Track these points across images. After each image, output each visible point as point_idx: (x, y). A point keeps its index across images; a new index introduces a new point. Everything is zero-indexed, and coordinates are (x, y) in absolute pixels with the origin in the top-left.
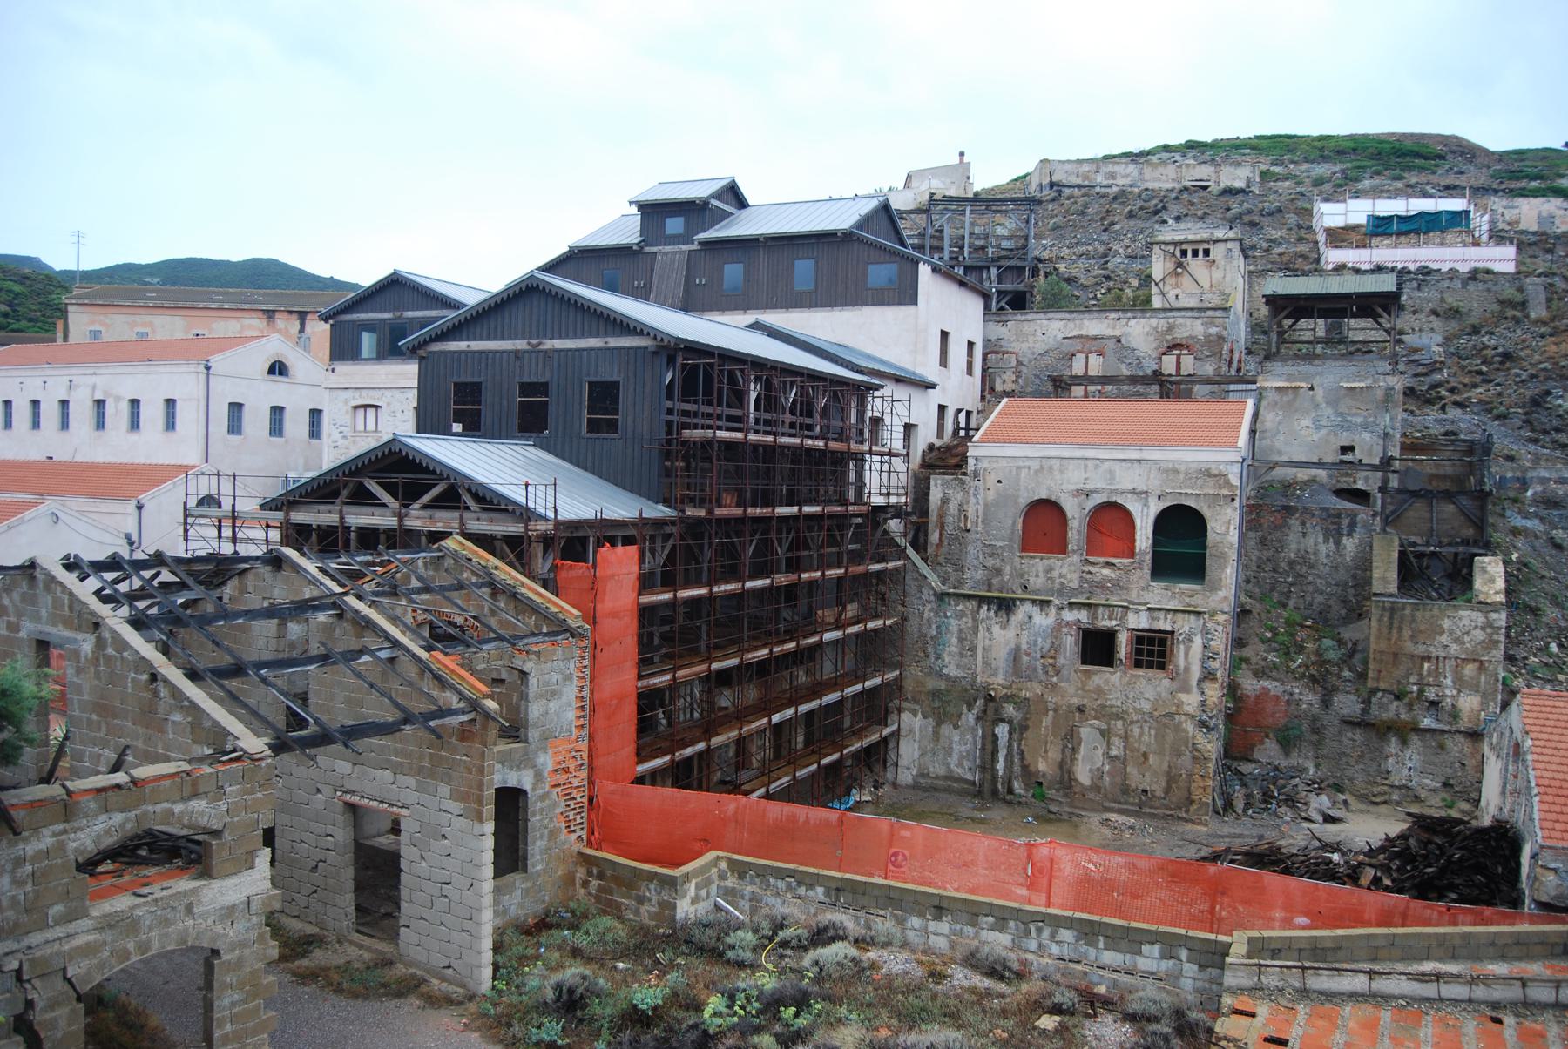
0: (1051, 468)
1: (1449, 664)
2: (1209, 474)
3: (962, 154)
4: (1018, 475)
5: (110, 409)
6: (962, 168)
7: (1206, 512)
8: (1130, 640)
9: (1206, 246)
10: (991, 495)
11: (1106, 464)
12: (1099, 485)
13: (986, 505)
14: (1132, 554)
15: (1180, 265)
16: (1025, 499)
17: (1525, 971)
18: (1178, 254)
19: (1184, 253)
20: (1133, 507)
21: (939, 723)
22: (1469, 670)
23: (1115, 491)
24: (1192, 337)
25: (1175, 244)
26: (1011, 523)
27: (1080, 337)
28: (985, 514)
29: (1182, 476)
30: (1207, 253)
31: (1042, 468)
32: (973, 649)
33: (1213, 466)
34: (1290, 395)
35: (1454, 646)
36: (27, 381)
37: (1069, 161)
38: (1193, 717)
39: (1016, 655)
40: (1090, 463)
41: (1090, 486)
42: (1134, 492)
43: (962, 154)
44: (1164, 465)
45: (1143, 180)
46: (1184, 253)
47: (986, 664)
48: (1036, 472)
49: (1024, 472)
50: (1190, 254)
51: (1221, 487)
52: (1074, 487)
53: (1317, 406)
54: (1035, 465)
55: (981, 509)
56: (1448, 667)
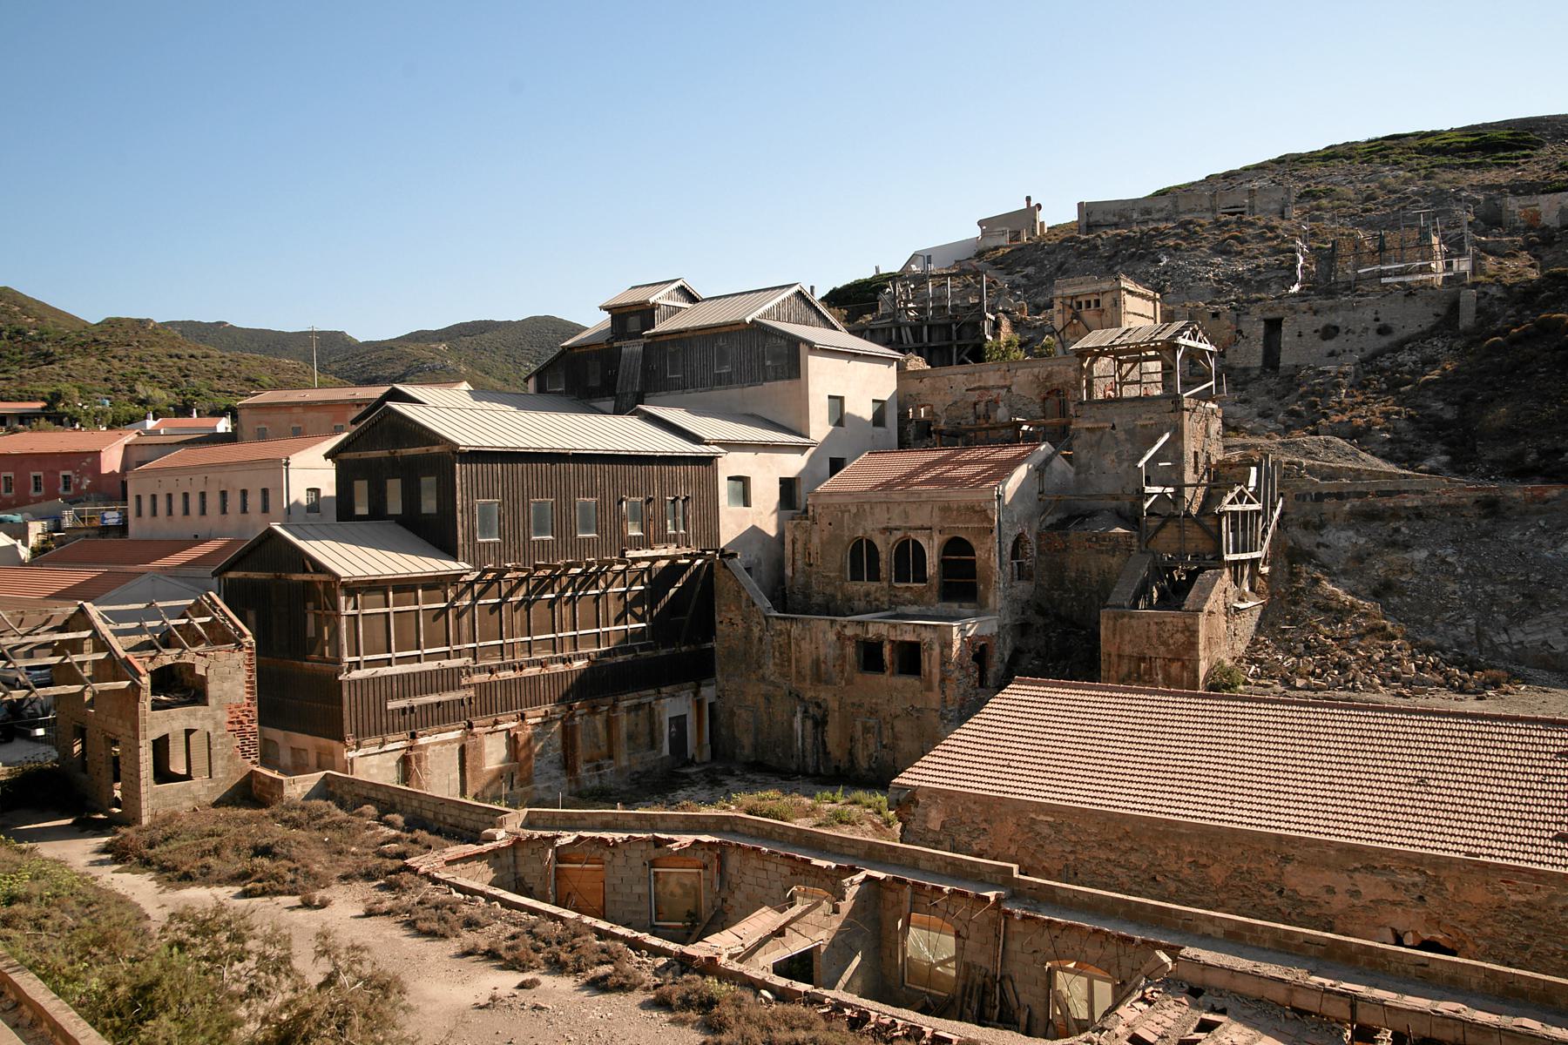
1: (1159, 662)
3: (1028, 199)
5: (209, 498)
6: (1031, 211)
7: (974, 544)
8: (892, 650)
14: (925, 580)
19: (1080, 304)
22: (1175, 668)
24: (1066, 383)
26: (840, 558)
27: (979, 388)
30: (1097, 303)
32: (789, 661)
34: (1095, 438)
35: (1162, 648)
36: (195, 478)
37: (1260, 168)
38: (696, 694)
39: (817, 663)
41: (892, 525)
42: (922, 528)
43: (1028, 199)
45: (1178, 213)
47: (798, 672)
53: (1117, 443)
56: (1159, 662)
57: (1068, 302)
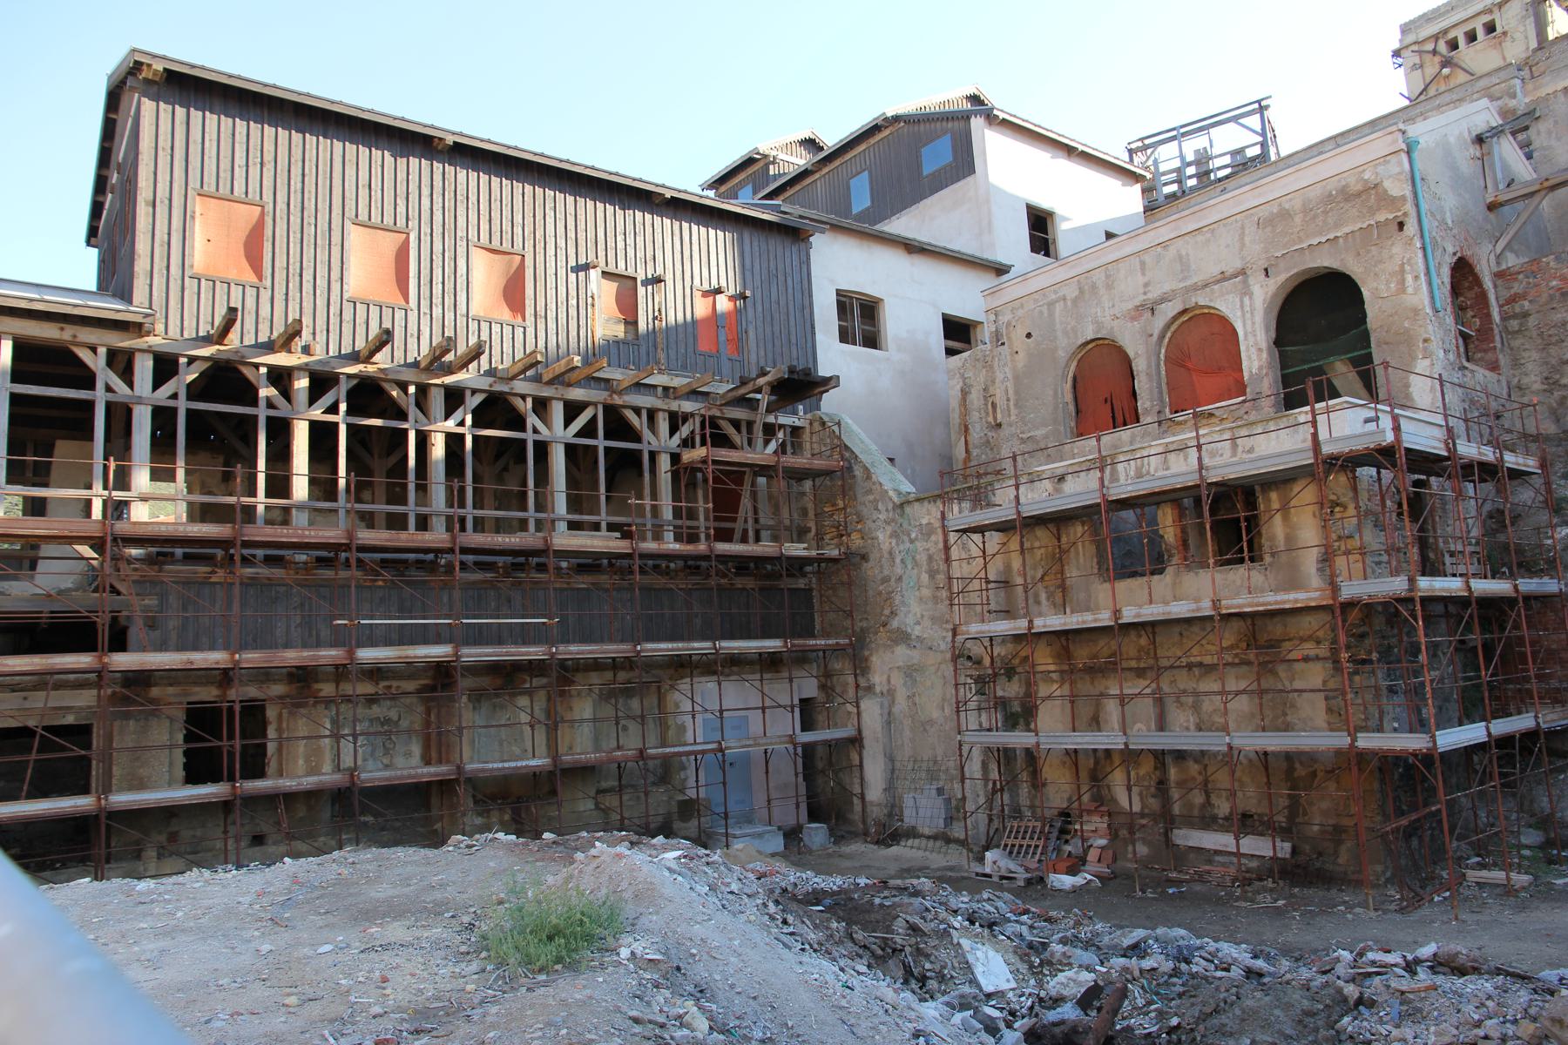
0: (1094, 287)
2: (1346, 196)
4: (1051, 314)
7: (1354, 268)
9: (1486, 18)
10: (1021, 359)
11: (1172, 251)
12: (1167, 287)
13: (1016, 378)
15: (1446, 63)
16: (1064, 346)
17: (398, 540)
18: (1442, 47)
19: (1453, 45)
20: (1227, 304)
21: (1552, 814)
23: (1195, 288)
25: (1436, 37)
28: (1017, 392)
29: (1298, 219)
30: (1490, 28)
31: (1081, 291)
33: (1352, 180)
40: (1147, 258)
41: (1154, 294)
42: (1223, 278)
44: (1263, 212)
46: (1453, 45)
48: (1075, 301)
49: (1059, 307)
50: (1462, 42)
51: (1372, 211)
52: (1130, 305)
54: (1071, 292)
55: (1010, 385)
57: (1430, 46)
